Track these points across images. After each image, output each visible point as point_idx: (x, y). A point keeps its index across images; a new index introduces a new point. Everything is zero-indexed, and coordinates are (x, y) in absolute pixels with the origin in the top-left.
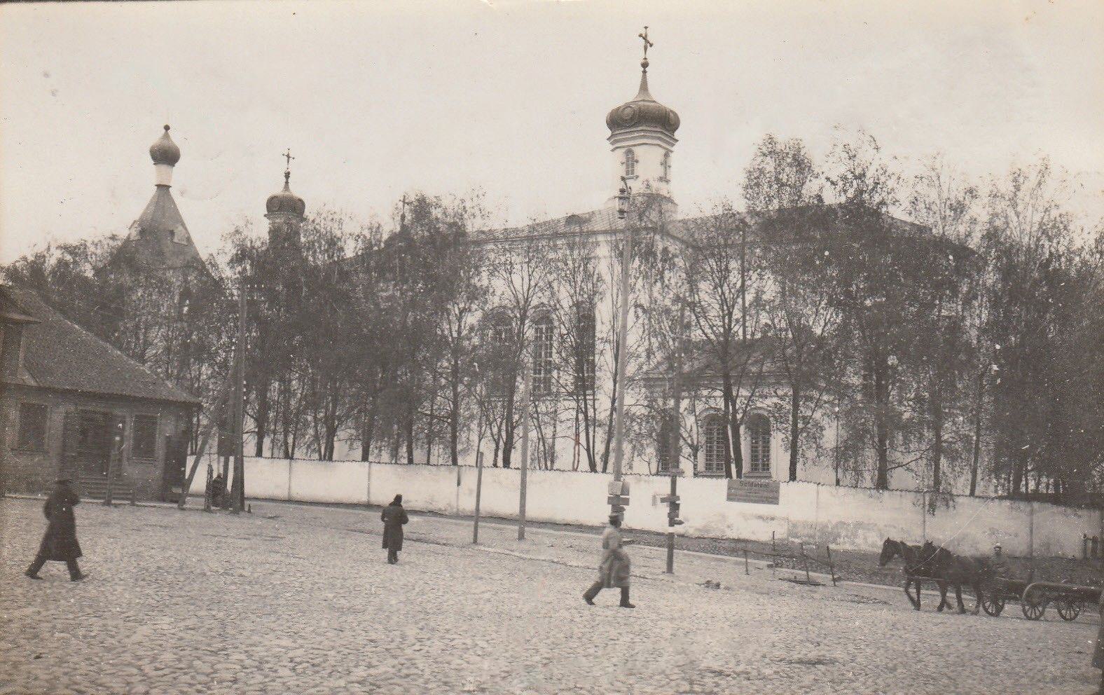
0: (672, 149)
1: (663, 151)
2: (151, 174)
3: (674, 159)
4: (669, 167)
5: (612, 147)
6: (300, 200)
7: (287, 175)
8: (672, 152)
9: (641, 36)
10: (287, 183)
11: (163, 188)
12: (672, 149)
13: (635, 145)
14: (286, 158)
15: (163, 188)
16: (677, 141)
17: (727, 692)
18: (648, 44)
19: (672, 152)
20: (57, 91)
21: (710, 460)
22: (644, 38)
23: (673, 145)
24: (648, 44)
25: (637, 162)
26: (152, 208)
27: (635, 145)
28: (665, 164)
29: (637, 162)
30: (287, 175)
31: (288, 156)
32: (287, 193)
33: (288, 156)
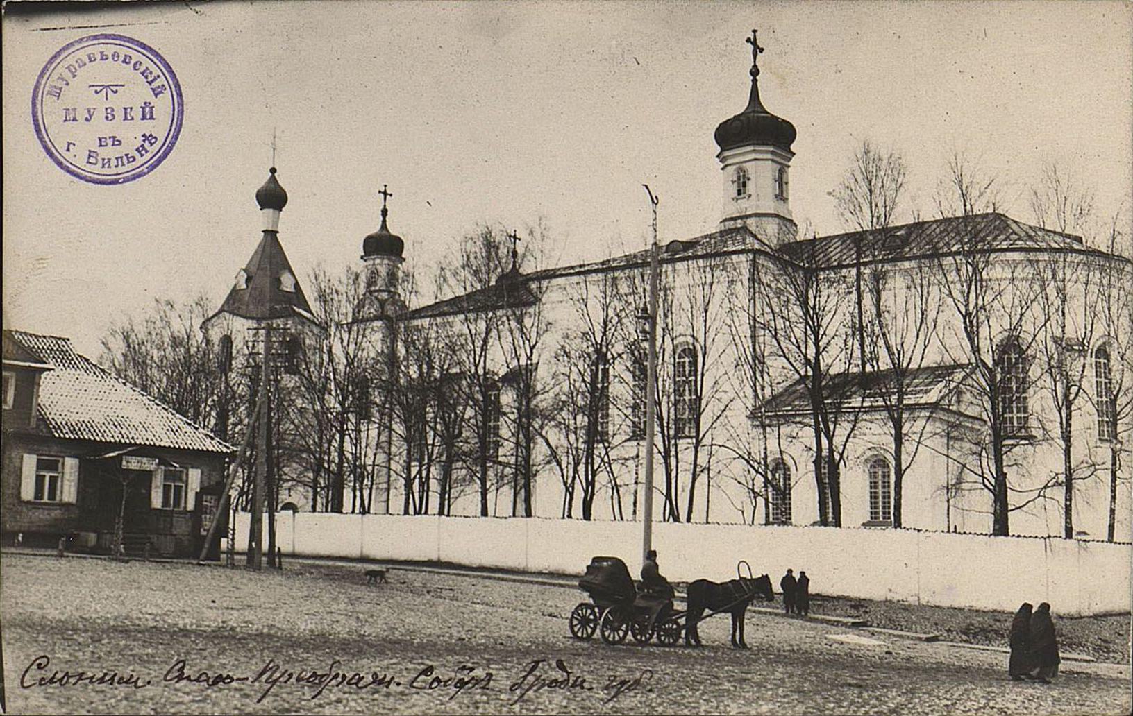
0: (790, 164)
1: (777, 167)
2: (261, 219)
3: (792, 174)
4: (787, 183)
5: (722, 165)
6: (399, 238)
7: (384, 212)
8: (789, 166)
9: (748, 40)
10: (384, 221)
11: (271, 235)
12: (790, 164)
13: (745, 162)
14: (382, 196)
15: (271, 235)
16: (794, 154)
17: (1131, 252)
18: (758, 49)
19: (789, 166)
20: (733, 199)
21: (876, 508)
22: (752, 43)
23: (789, 160)
24: (758, 49)
25: (749, 179)
26: (257, 260)
27: (745, 162)
28: (781, 181)
29: (749, 179)
30: (384, 212)
31: (385, 193)
32: (384, 232)
33: (385, 193)
